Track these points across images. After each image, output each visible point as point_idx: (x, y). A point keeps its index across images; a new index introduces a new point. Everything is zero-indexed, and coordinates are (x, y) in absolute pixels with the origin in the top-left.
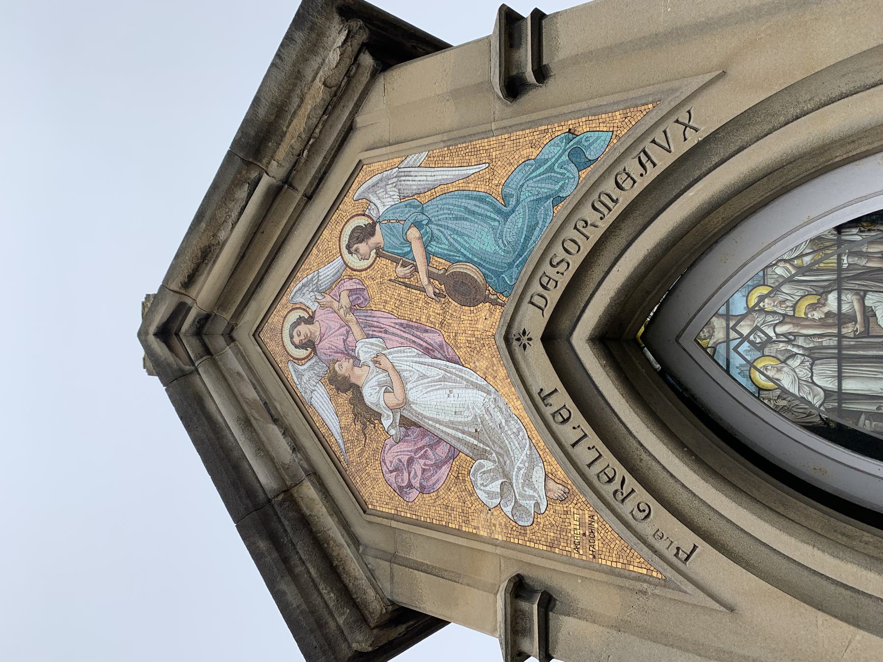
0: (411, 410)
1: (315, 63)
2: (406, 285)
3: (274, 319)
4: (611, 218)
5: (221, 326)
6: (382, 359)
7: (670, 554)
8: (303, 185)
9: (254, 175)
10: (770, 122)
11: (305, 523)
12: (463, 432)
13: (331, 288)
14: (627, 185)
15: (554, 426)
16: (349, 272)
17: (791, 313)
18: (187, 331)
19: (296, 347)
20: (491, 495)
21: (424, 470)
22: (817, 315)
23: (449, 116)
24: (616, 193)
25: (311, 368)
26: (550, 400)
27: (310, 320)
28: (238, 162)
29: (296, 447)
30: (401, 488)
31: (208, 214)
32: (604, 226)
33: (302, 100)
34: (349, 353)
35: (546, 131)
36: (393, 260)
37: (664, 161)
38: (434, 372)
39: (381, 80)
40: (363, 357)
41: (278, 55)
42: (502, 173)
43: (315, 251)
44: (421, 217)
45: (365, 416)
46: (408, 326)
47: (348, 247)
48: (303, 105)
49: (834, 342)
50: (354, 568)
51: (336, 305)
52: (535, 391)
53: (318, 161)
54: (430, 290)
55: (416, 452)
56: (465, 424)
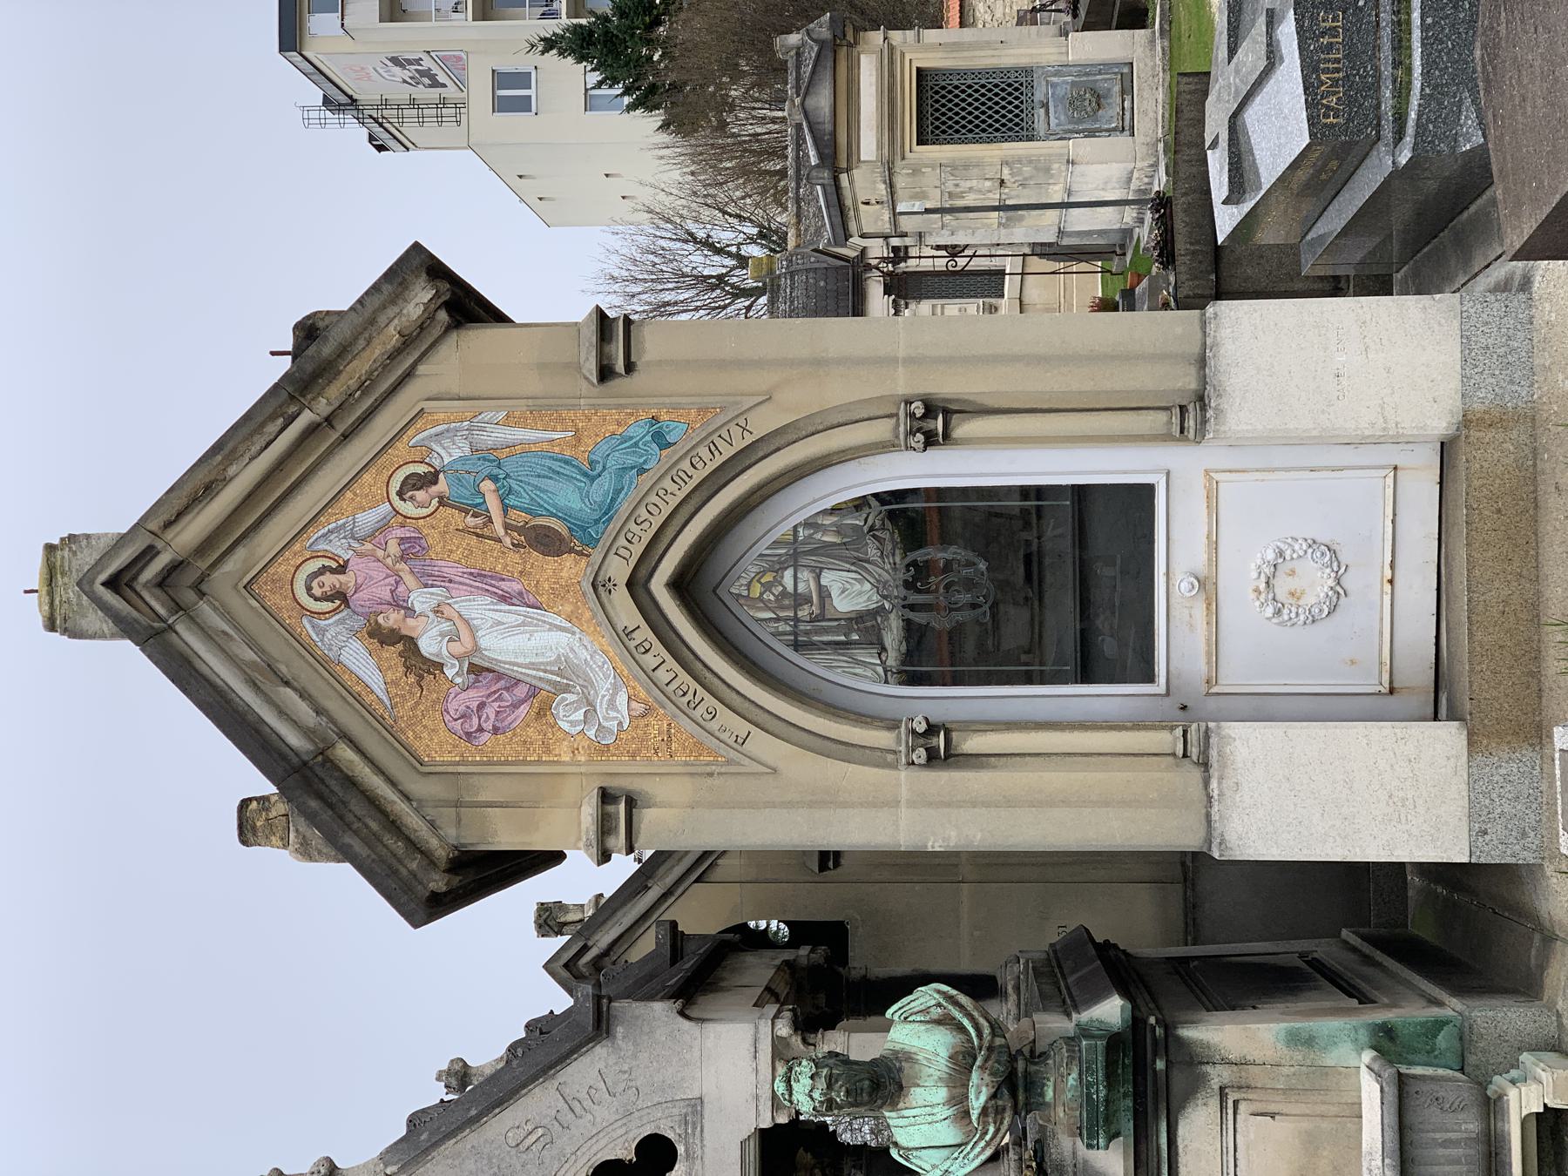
0: (483, 657)
2: (478, 535)
3: (282, 569)
4: (687, 489)
6: (447, 611)
7: (731, 742)
8: (342, 427)
9: (293, 409)
11: (351, 782)
12: (545, 671)
13: (372, 535)
14: (700, 465)
15: (637, 656)
16: (400, 519)
17: (745, 593)
19: (316, 599)
20: (573, 724)
23: (533, 385)
24: (691, 471)
25: (338, 622)
27: (342, 569)
28: (284, 395)
29: (319, 711)
30: (468, 734)
31: (230, 446)
32: (681, 495)
33: (369, 343)
34: (399, 603)
36: (461, 510)
37: (728, 452)
38: (511, 619)
39: (454, 336)
41: (360, 301)
42: (588, 443)
43: (349, 495)
44: (496, 471)
45: (420, 666)
47: (400, 494)
51: (380, 553)
52: (620, 628)
54: (507, 541)
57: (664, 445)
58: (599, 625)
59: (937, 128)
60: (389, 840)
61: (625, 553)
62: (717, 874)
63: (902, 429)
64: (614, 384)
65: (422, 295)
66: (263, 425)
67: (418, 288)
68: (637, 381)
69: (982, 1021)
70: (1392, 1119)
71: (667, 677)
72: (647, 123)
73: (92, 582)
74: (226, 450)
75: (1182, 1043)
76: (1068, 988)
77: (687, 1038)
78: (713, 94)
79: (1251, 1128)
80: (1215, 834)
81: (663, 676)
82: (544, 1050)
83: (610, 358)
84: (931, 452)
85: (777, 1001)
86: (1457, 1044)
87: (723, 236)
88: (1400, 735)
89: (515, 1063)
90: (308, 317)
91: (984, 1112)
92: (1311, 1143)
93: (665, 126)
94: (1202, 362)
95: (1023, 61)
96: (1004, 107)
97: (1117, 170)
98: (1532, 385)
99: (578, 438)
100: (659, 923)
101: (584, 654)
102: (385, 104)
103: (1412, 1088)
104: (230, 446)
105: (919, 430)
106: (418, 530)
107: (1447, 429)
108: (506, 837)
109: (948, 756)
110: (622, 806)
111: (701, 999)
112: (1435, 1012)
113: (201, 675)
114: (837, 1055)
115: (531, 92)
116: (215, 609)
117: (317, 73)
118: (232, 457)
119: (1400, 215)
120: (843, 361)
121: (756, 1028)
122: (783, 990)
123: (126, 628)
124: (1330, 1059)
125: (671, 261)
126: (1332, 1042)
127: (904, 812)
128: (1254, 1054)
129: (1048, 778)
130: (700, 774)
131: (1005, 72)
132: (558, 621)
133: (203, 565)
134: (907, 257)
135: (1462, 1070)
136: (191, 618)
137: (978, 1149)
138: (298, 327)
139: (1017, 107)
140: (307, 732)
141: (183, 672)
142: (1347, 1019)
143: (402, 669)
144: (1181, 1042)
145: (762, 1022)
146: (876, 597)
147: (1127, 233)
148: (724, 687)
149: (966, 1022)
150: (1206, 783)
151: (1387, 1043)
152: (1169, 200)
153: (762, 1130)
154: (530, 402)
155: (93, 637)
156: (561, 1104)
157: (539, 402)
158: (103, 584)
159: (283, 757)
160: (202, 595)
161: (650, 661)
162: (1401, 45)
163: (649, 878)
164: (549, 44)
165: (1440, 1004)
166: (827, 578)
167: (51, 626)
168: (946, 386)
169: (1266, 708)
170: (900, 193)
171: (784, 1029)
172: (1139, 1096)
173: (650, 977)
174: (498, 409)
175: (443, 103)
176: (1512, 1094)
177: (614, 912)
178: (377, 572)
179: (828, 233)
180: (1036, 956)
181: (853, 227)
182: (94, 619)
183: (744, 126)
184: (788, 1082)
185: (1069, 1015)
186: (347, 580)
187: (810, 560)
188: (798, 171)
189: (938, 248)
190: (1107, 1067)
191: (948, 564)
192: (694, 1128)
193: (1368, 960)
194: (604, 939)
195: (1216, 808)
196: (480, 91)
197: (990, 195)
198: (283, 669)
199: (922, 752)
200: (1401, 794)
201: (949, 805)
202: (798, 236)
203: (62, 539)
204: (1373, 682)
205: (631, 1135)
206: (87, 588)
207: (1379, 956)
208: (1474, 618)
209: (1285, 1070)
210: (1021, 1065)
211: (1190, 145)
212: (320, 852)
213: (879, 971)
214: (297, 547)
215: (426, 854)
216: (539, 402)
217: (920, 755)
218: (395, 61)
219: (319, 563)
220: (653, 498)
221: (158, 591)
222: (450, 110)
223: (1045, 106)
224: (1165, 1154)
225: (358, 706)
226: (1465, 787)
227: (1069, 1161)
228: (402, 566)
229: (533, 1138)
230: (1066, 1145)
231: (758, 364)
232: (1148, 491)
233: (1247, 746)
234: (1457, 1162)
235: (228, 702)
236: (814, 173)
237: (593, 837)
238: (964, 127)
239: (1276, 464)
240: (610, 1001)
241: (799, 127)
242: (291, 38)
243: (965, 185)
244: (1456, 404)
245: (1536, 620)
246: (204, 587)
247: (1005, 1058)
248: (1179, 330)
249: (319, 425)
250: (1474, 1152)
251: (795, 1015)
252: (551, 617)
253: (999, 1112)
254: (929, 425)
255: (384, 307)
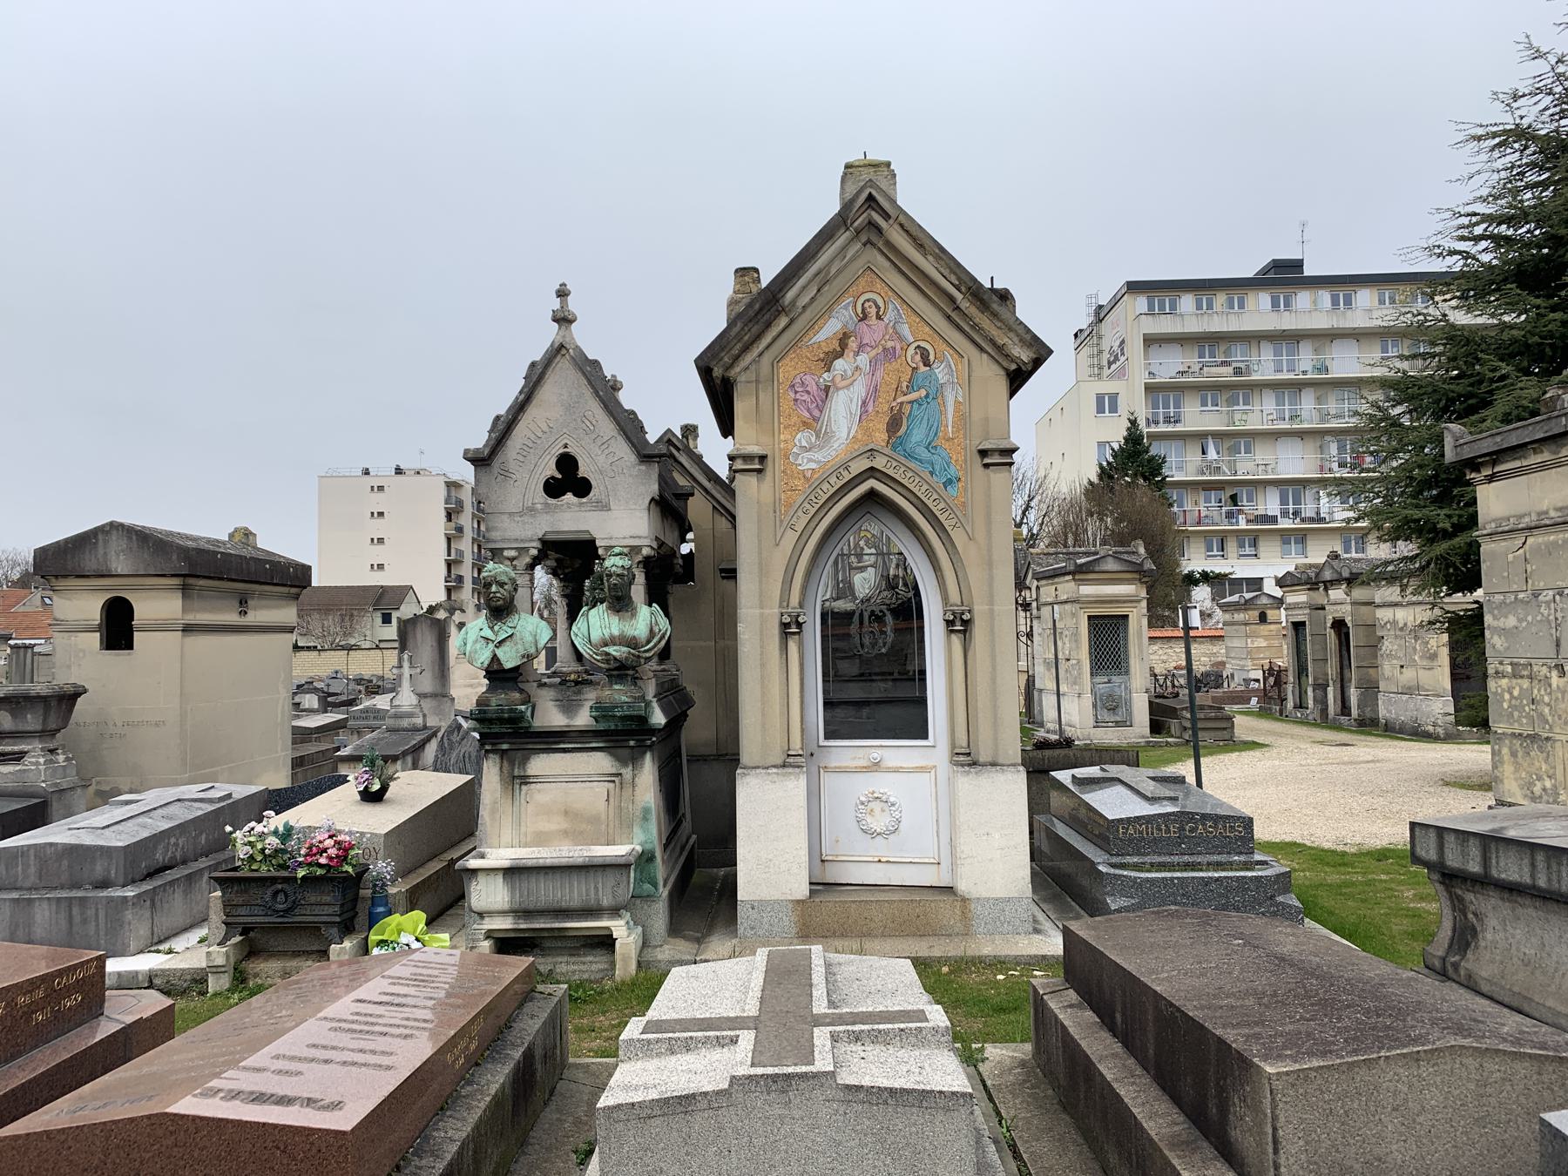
1: (1016, 339)
3: (879, 286)
5: (874, 239)
11: (768, 325)
22: (862, 543)
23: (977, 416)
27: (879, 317)
34: (861, 347)
39: (1003, 373)
53: (967, 328)
60: (739, 346)
62: (717, 516)
65: (1025, 355)
70: (608, 861)
72: (1093, 474)
74: (941, 254)
79: (601, 789)
81: (825, 486)
82: (630, 426)
84: (943, 624)
87: (1032, 515)
91: (607, 654)
92: (594, 820)
93: (1091, 483)
94: (994, 764)
95: (1132, 670)
97: (1075, 719)
99: (948, 440)
102: (1100, 337)
112: (661, 883)
117: (1115, 302)
118: (937, 258)
119: (1066, 866)
122: (663, 550)
123: (846, 206)
124: (637, 830)
126: (646, 830)
129: (776, 686)
131: (1127, 661)
133: (880, 245)
147: (1041, 725)
151: (646, 858)
161: (833, 480)
162: (1161, 867)
164: (1133, 422)
168: (979, 632)
169: (814, 796)
171: (646, 551)
175: (1101, 368)
176: (622, 922)
179: (1039, 569)
181: (1043, 582)
182: (852, 189)
183: (1092, 527)
186: (873, 320)
193: (683, 848)
194: (683, 459)
196: (1107, 387)
204: (827, 852)
207: (685, 854)
213: (671, 600)
215: (731, 366)
218: (1123, 342)
219: (881, 304)
222: (1097, 373)
230: (590, 696)
232: (924, 735)
233: (794, 787)
242: (1134, 287)
244: (974, 895)
245: (862, 935)
252: (855, 427)
253: (608, 661)
254: (958, 622)
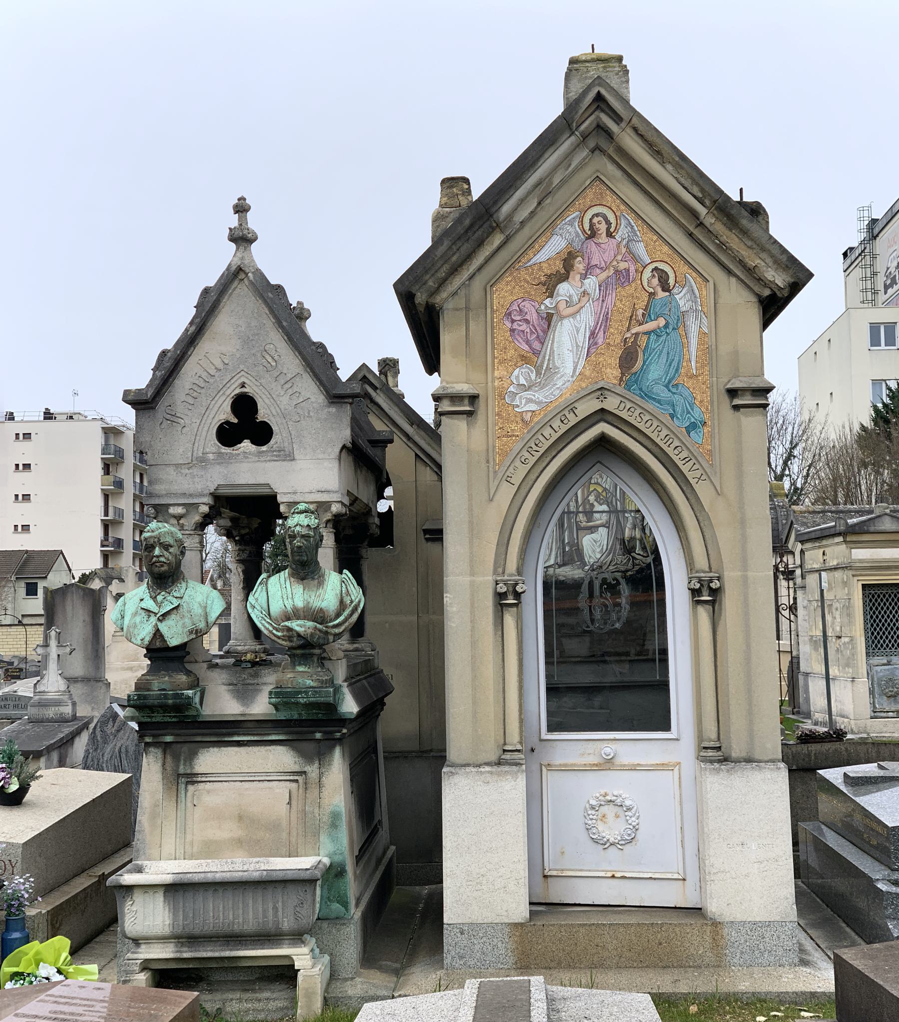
1: (769, 261)
2: (631, 317)
3: (609, 198)
5: (603, 144)
6: (585, 299)
7: (508, 474)
8: (697, 233)
9: (707, 202)
10: (635, 615)
11: (480, 244)
14: (676, 452)
15: (559, 416)
16: (641, 269)
17: (593, 482)
18: (601, 119)
19: (591, 220)
20: (517, 378)
21: (523, 331)
22: (592, 498)
23: (725, 349)
25: (577, 233)
26: (572, 413)
27: (610, 235)
30: (510, 314)
31: (685, 166)
32: (658, 441)
35: (707, 409)
36: (646, 306)
37: (685, 469)
38: (581, 338)
40: (587, 281)
41: (776, 241)
43: (655, 238)
44: (671, 327)
46: (607, 318)
47: (656, 269)
48: (745, 248)
49: (572, 509)
50: (457, 282)
51: (619, 257)
52: (576, 405)
53: (712, 247)
55: (533, 326)
56: (554, 361)
57: (688, 430)
58: (578, 392)
59: (873, 596)
60: (446, 268)
61: (621, 408)
62: (420, 467)
63: (702, 575)
64: (725, 398)
66: (698, 184)
67: (784, 276)
68: (728, 413)
69: (343, 628)
70: (290, 876)
71: (546, 434)
72: (865, 417)
73: (599, 85)
74: (682, 163)
75: (331, 749)
76: (360, 680)
77: (330, 450)
78: (884, 459)
79: (282, 790)
80: (457, 769)
81: (547, 432)
83: (742, 395)
84: (687, 594)
85: (351, 505)
86: (333, 915)
87: (795, 466)
88: (520, 881)
89: (313, 347)
90: (764, 210)
91: (290, 629)
92: (274, 826)
93: (863, 428)
94: (749, 760)
96: (887, 637)
98: (740, 966)
99: (692, 377)
100: (392, 432)
101: (560, 383)
102: (874, 257)
103: (308, 888)
104: (685, 166)
105: (702, 585)
106: (634, 280)
107: (711, 911)
108: (448, 339)
109: (502, 605)
110: (468, 408)
111: (351, 458)
112: (353, 902)
113: (543, 153)
114: (321, 541)
115: (883, 346)
116: (584, 159)
119: (839, 884)
120: (744, 538)
121: (336, 492)
123: (571, 107)
124: (324, 838)
125: (779, 433)
126: (334, 840)
127: (468, 579)
128: (326, 793)
129: (490, 667)
130: (488, 455)
132: (580, 368)
133: (611, 151)
134: (788, 579)
135: (318, 919)
136: (578, 145)
137: (267, 626)
138: (758, 204)
139: (887, 646)
140: (510, 216)
141: (547, 141)
142: (347, 848)
143: (549, 272)
144: (332, 748)
145: (340, 495)
146: (592, 561)
147: (808, 715)
148: (541, 469)
149: (342, 618)
150: (488, 764)
151: (334, 872)
152: (841, 740)
153: (276, 496)
154: (714, 347)
155: (566, 86)
156: (289, 376)
157: (714, 353)
158: (599, 92)
159: (495, 203)
160: (593, 151)
161: (556, 423)
163: (418, 426)
165: (357, 905)
166: (603, 531)
167: (573, 61)
168: (730, 602)
169: (535, 800)
170: (831, 574)
171: (336, 508)
172: (300, 723)
173: (361, 428)
174: (709, 328)
175: (875, 293)
176: (305, 950)
177: (397, 405)
178: (608, 256)
179: (803, 530)
180: (376, 661)
181: (808, 545)
182: (577, 87)
183: (865, 479)
184: (305, 511)
185: (345, 681)
186: (603, 238)
187: (613, 520)
188: (842, 512)
189: (795, 599)
190: (317, 703)
191: (619, 605)
192: (276, 456)
193: (379, 862)
194: (381, 399)
195: (473, 770)
197: (831, 630)
198: (548, 201)
199: (504, 589)
200: (484, 882)
201: (472, 606)
202: (801, 512)
203: (626, 66)
204: (551, 865)
205: (272, 419)
206: (596, 82)
207: (382, 868)
208: (594, 928)
209: (316, 811)
210: (317, 651)
211: (878, 752)
212: (438, 226)
213: (365, 567)
214: (623, 207)
215: (437, 291)
216: (714, 353)
217: (502, 588)
220: (655, 424)
221: (594, 125)
222: (871, 296)
223: (889, 663)
224: (266, 738)
225: (526, 246)
226: (490, 921)
227: (260, 681)
228: (612, 271)
229: (270, 360)
231: (740, 487)
232: (667, 727)
233: (512, 788)
234: (265, 916)
235: (528, 169)
236: (842, 522)
237: (449, 391)
238: (874, 613)
239: (684, 806)
240: (351, 404)
241: (870, 512)
243: (837, 614)
245: (593, 966)
246: (597, 152)
247: (321, 641)
248: (769, 746)
249: (698, 219)
250: (271, 926)
251: (343, 515)
252: (582, 362)
253: (290, 638)
254: (705, 591)
255: (772, 256)
